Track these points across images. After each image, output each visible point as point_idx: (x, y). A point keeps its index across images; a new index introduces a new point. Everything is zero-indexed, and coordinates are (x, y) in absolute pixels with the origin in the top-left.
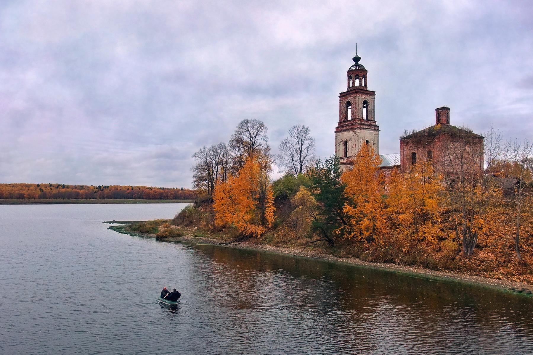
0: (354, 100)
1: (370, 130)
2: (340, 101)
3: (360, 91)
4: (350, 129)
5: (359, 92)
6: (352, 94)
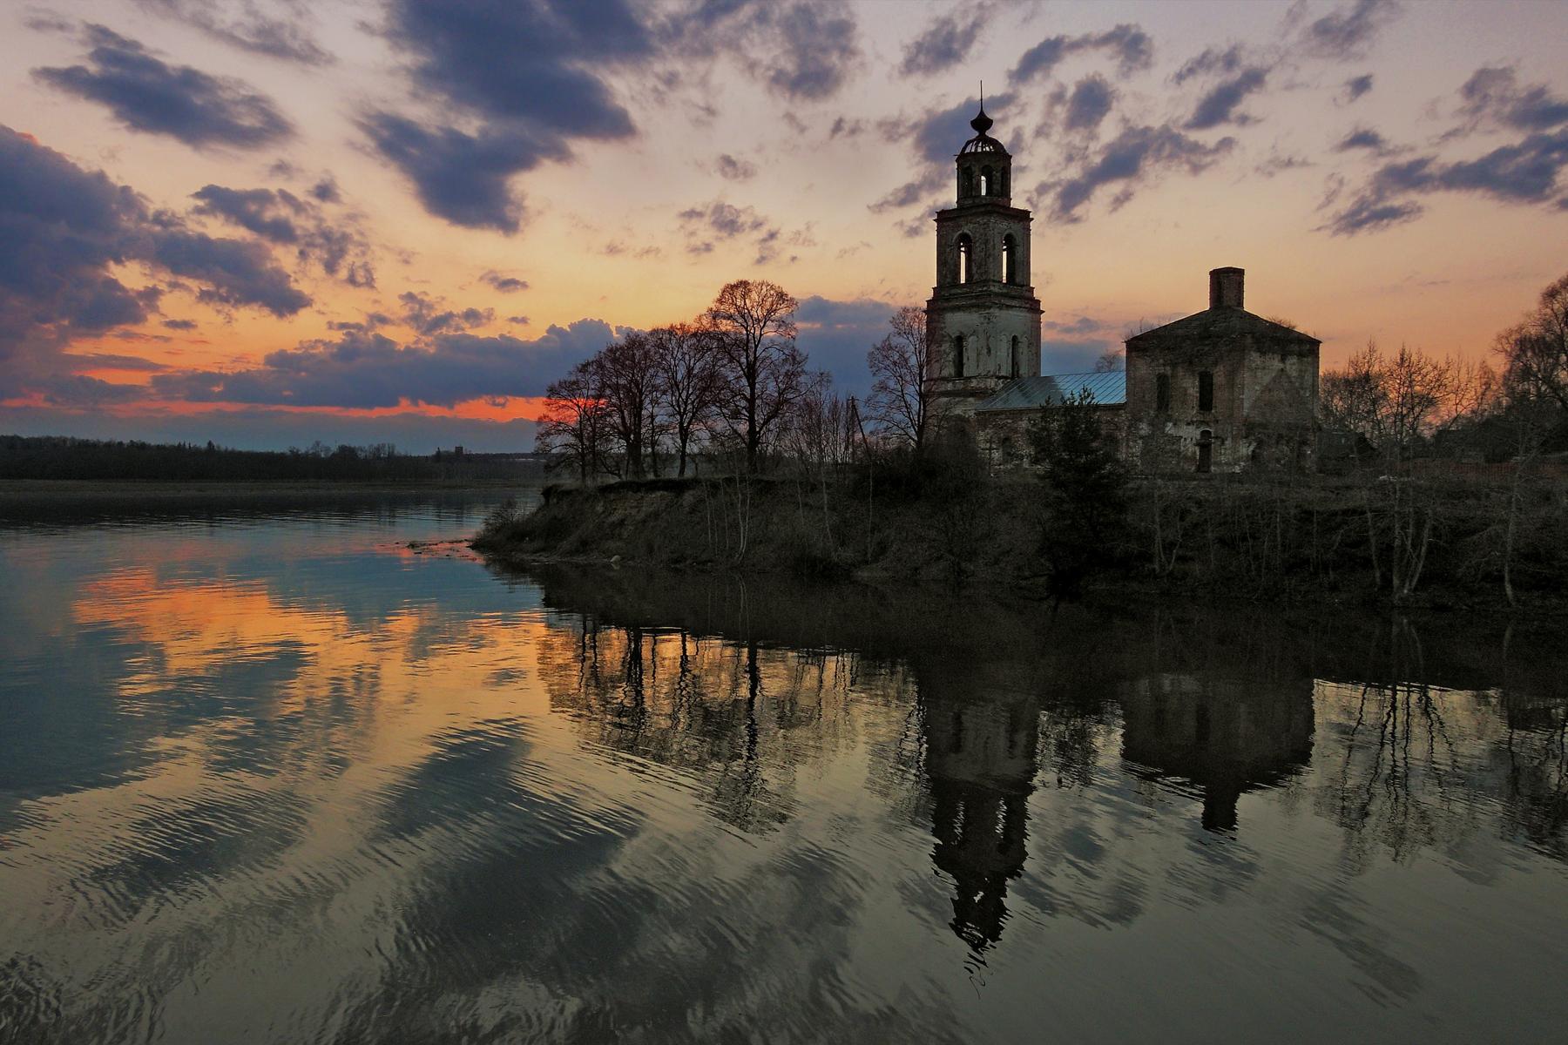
0: (982, 231)
1: (1021, 311)
3: (997, 209)
4: (973, 306)
6: (976, 214)
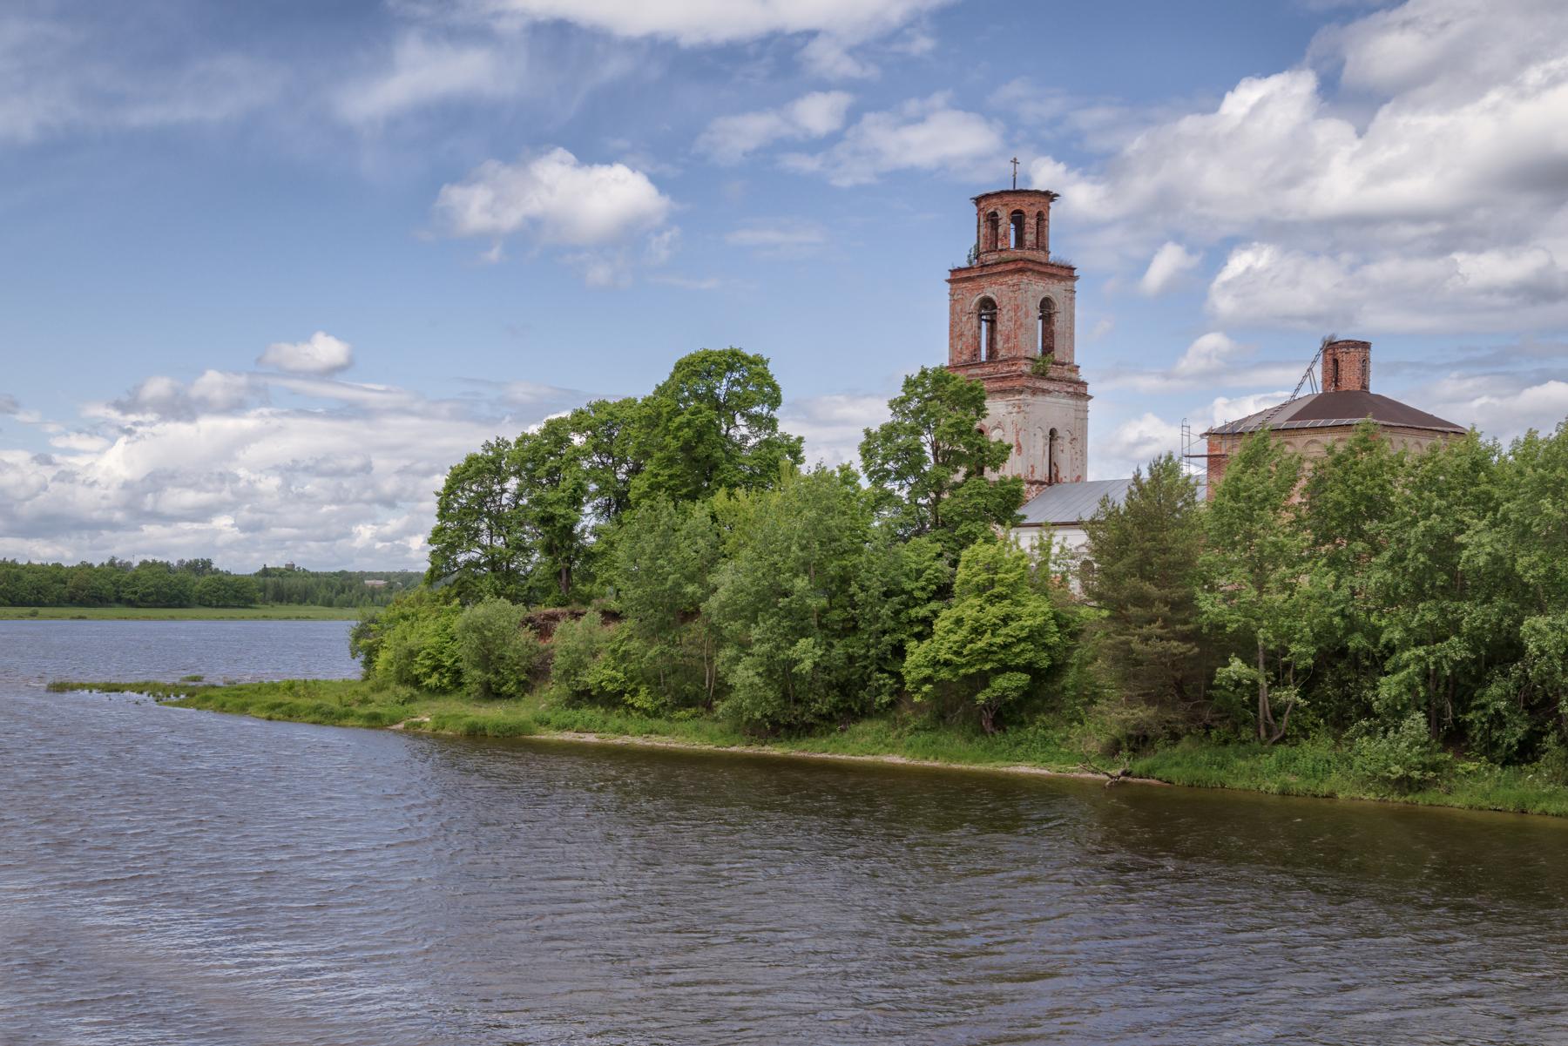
2: (952, 295)
5: (1030, 270)
